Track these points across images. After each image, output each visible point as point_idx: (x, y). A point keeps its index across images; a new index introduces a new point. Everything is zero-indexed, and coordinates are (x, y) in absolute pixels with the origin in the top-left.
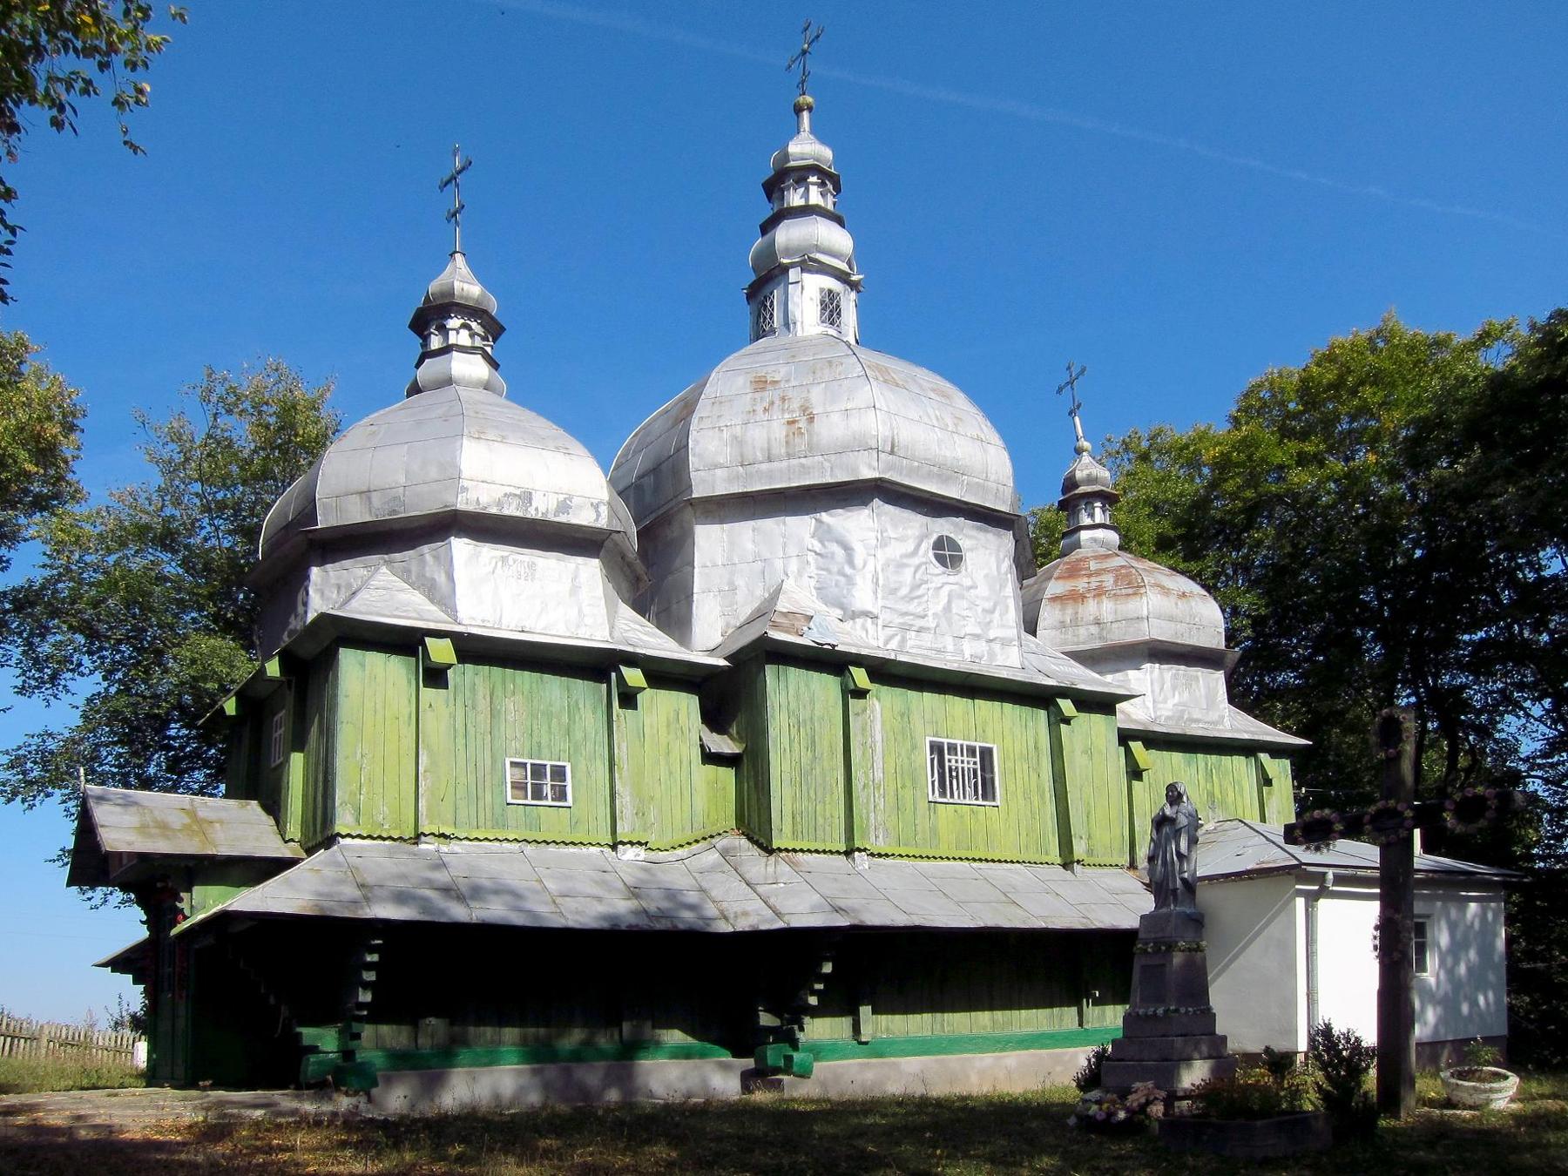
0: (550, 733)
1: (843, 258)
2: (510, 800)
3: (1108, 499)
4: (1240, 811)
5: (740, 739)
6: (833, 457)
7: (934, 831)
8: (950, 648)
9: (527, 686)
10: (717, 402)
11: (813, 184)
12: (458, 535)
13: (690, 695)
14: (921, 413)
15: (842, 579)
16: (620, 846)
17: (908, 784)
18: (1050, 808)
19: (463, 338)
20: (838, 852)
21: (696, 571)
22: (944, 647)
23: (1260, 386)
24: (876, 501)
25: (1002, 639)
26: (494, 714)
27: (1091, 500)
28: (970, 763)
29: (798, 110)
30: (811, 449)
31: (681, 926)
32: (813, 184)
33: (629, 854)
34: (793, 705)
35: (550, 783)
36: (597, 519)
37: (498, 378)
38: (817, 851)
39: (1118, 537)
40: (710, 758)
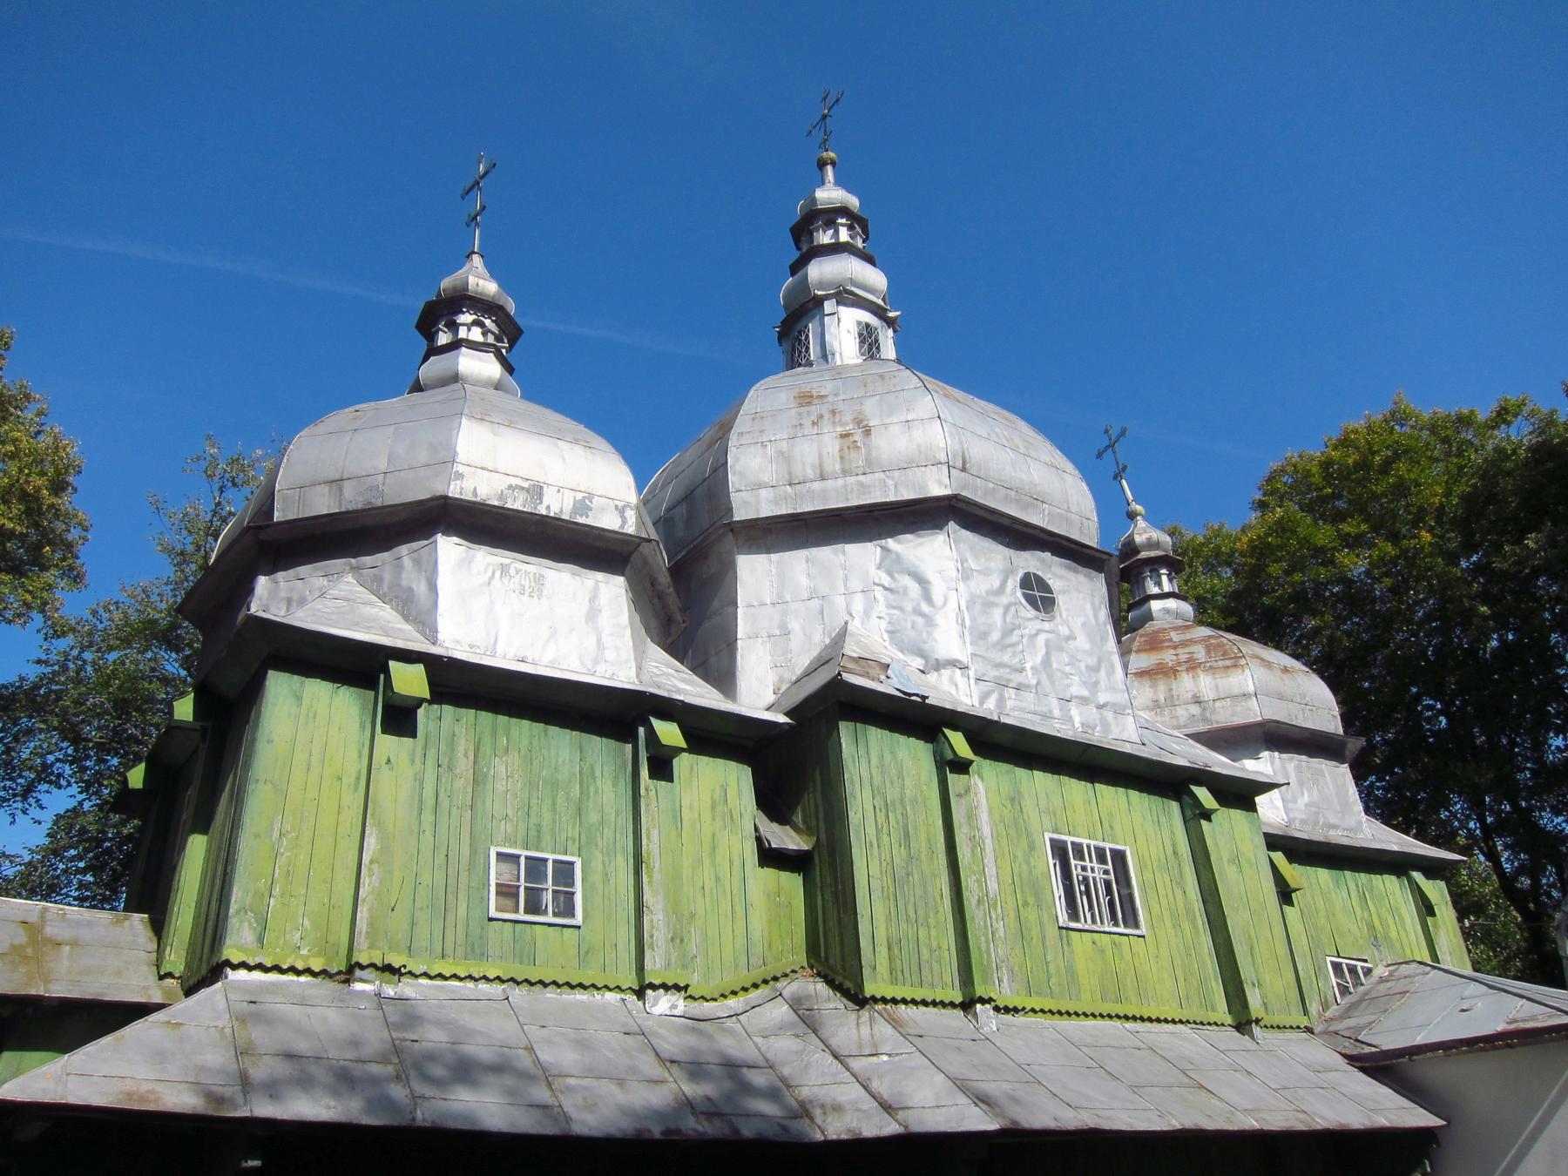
0: (554, 810)
1: (878, 294)
2: (493, 913)
3: (1173, 565)
4: (1408, 951)
5: (807, 830)
6: (896, 474)
7: (1071, 972)
8: (1057, 713)
9: (525, 742)
10: (756, 416)
11: (843, 225)
12: (447, 533)
13: (741, 766)
14: (989, 431)
15: (920, 620)
16: (649, 992)
17: (1031, 900)
18: (1206, 941)
19: (476, 335)
20: (952, 1005)
21: (740, 611)
22: (1050, 712)
23: (1283, 471)
24: (952, 526)
25: (1114, 705)
26: (478, 780)
27: (1156, 567)
28: (1098, 873)
29: (822, 164)
30: (870, 466)
31: (748, 1131)
32: (843, 225)
33: (662, 1004)
34: (877, 780)
35: (551, 888)
36: (622, 526)
37: (511, 381)
38: (925, 1003)
39: (1191, 609)
40: (770, 857)
